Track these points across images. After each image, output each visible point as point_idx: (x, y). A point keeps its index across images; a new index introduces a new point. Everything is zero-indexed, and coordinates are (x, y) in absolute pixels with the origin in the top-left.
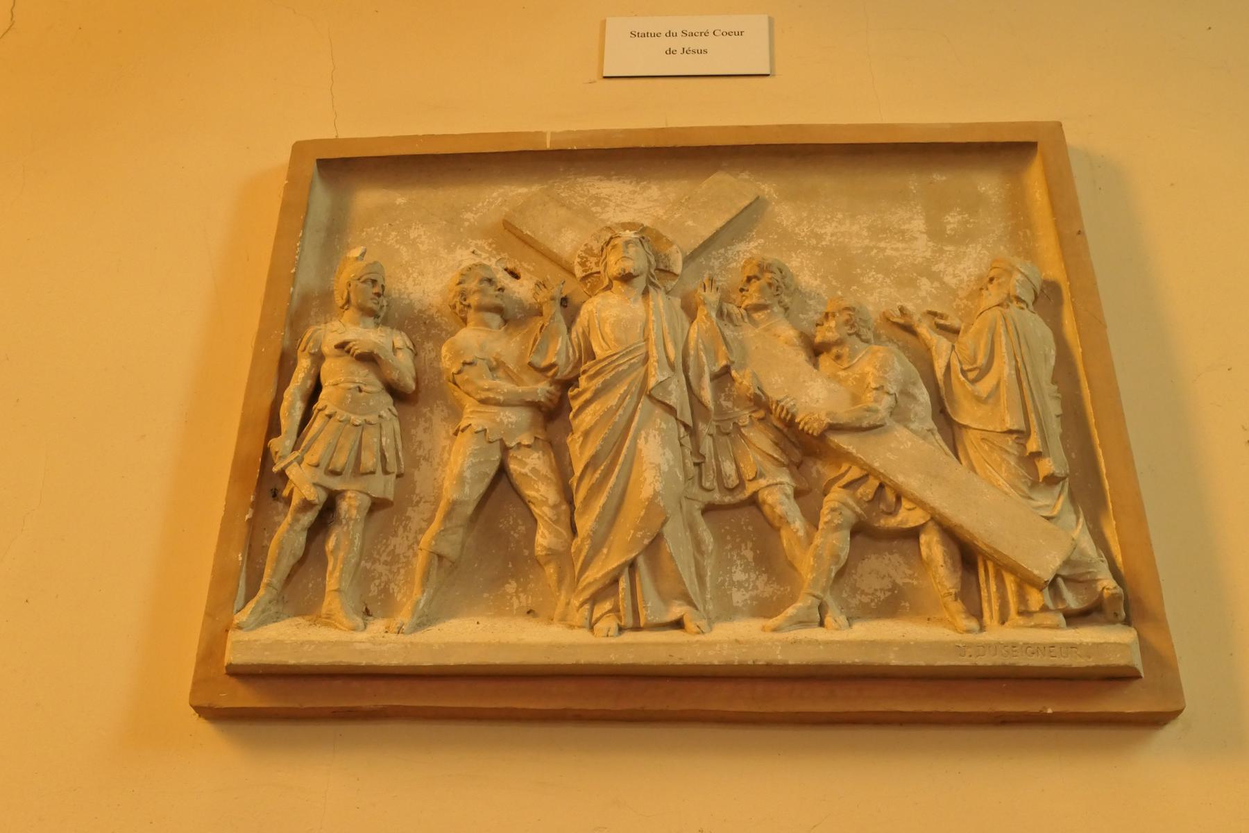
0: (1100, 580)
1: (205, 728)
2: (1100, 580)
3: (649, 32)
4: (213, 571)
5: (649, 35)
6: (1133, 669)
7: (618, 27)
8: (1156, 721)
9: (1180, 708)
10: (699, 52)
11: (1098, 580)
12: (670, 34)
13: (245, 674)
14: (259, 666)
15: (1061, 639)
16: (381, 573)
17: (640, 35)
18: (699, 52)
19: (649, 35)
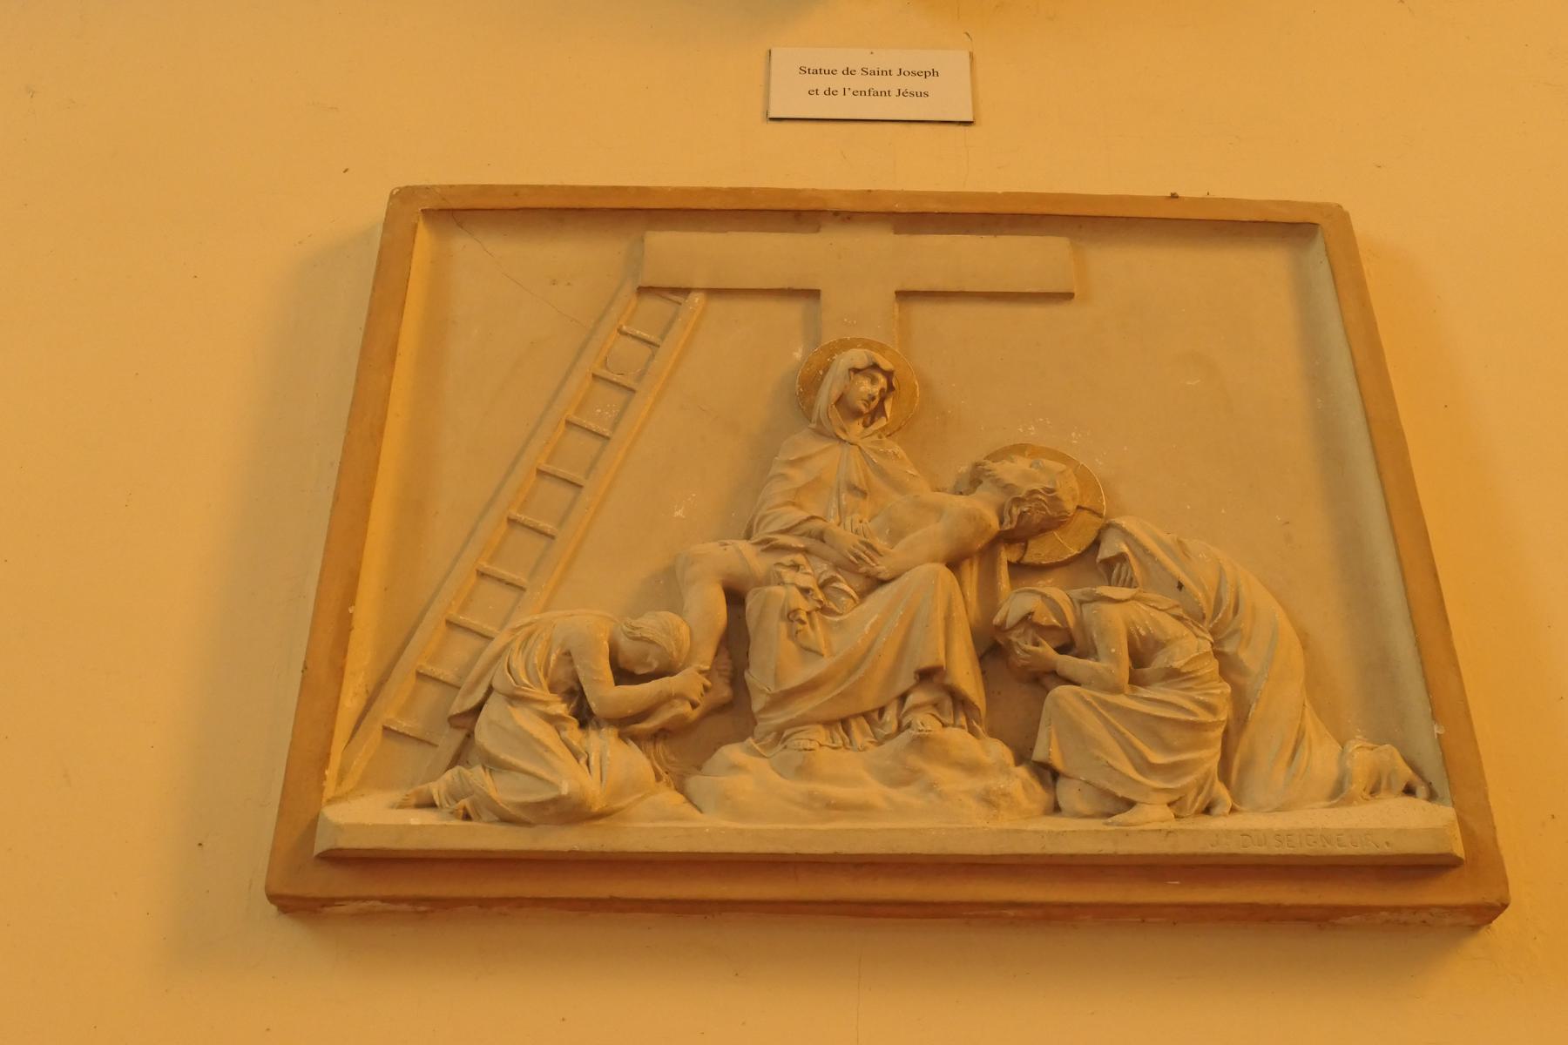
0: (655, 748)
1: (291, 932)
2: (655, 748)
3: (818, 69)
4: (673, 717)
5: (823, 71)
6: (1451, 856)
7: (787, 59)
8: (1486, 913)
9: (1492, 899)
10: (919, 94)
11: (655, 744)
12: (848, 72)
13: (337, 859)
14: (463, 851)
15: (1280, 822)
16: (583, 725)
17: (811, 71)
18: (919, 94)
19: (823, 71)
